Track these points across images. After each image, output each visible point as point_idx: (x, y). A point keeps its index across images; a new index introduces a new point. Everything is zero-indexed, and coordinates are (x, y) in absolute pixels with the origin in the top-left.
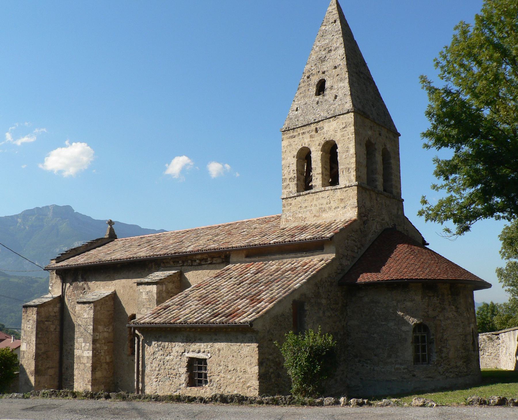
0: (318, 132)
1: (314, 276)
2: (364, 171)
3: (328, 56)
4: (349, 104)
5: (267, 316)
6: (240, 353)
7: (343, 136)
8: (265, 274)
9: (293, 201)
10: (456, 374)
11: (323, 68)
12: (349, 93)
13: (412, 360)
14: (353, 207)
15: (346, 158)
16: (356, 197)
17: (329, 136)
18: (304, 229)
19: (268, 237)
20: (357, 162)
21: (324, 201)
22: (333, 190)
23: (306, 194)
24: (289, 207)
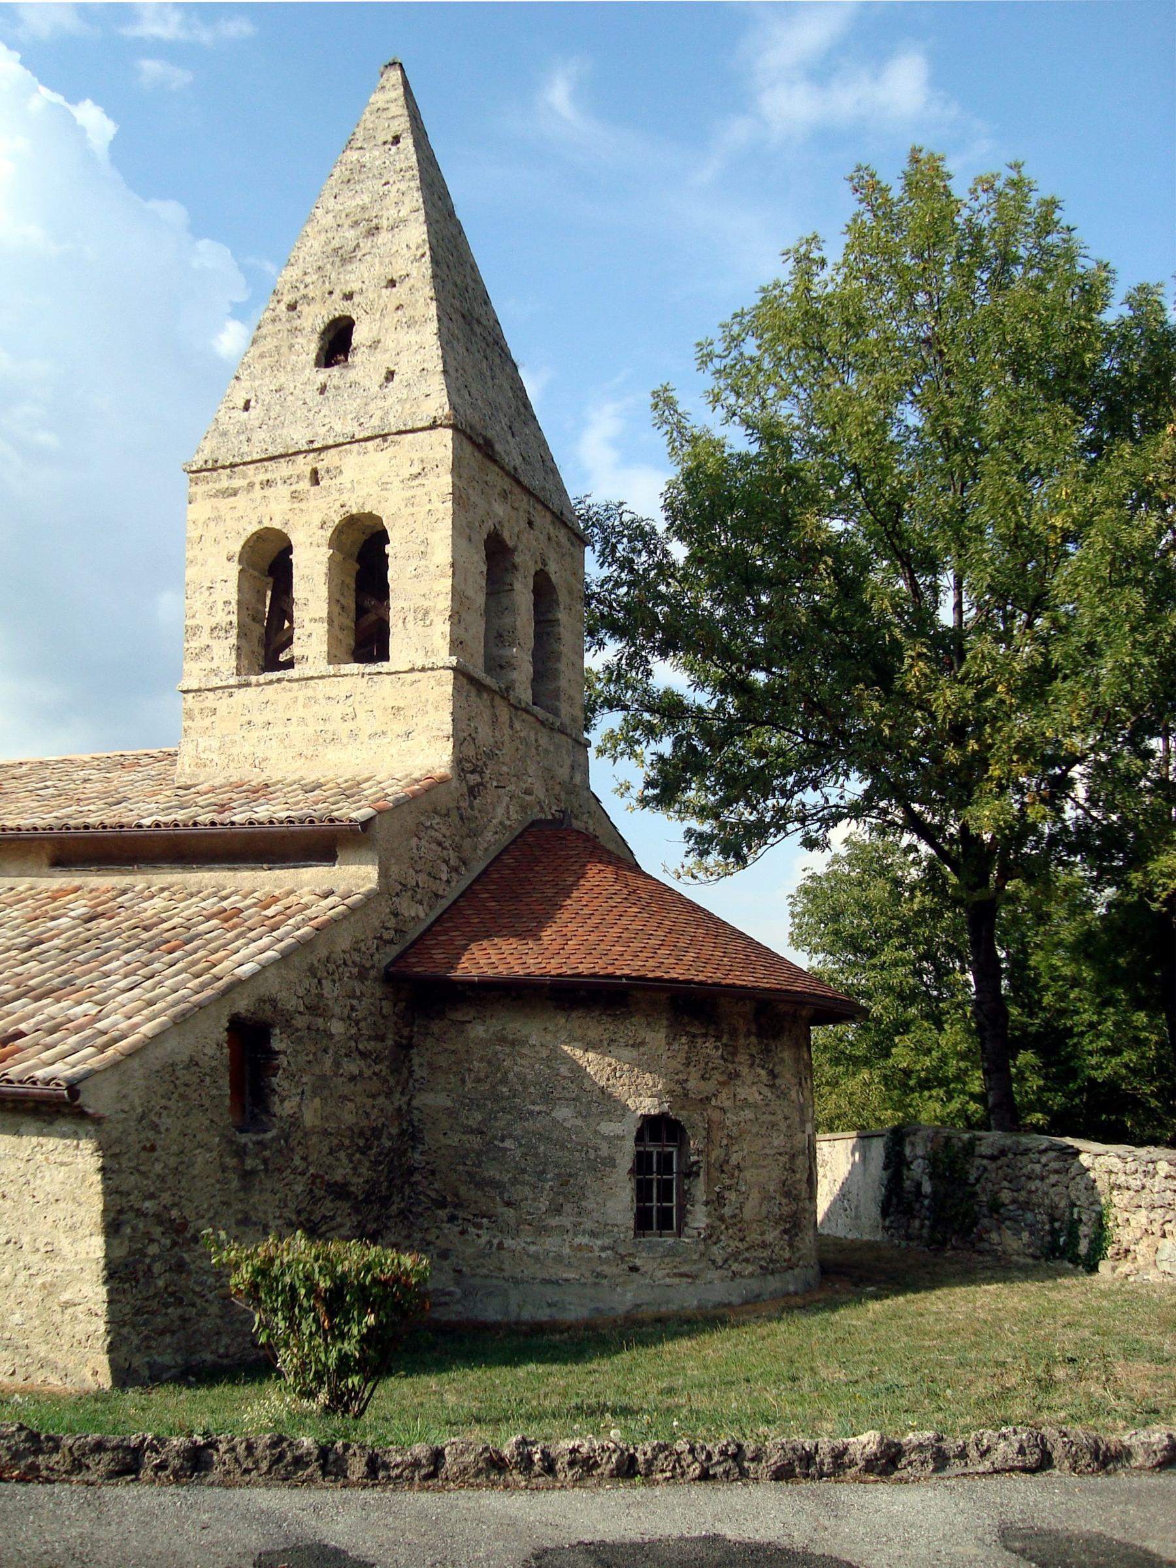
0: (322, 483)
1: (304, 945)
2: (478, 627)
3: (366, 245)
4: (439, 400)
5: (135, 1063)
6: (32, 1186)
7: (410, 502)
8: (122, 922)
9: (223, 703)
10: (761, 1267)
11: (347, 282)
12: (440, 367)
13: (631, 1223)
14: (436, 738)
15: (416, 577)
16: (448, 707)
17: (361, 501)
18: (262, 791)
19: (131, 807)
20: (457, 594)
21: (337, 711)
22: (366, 677)
23: (271, 682)
24: (207, 722)
